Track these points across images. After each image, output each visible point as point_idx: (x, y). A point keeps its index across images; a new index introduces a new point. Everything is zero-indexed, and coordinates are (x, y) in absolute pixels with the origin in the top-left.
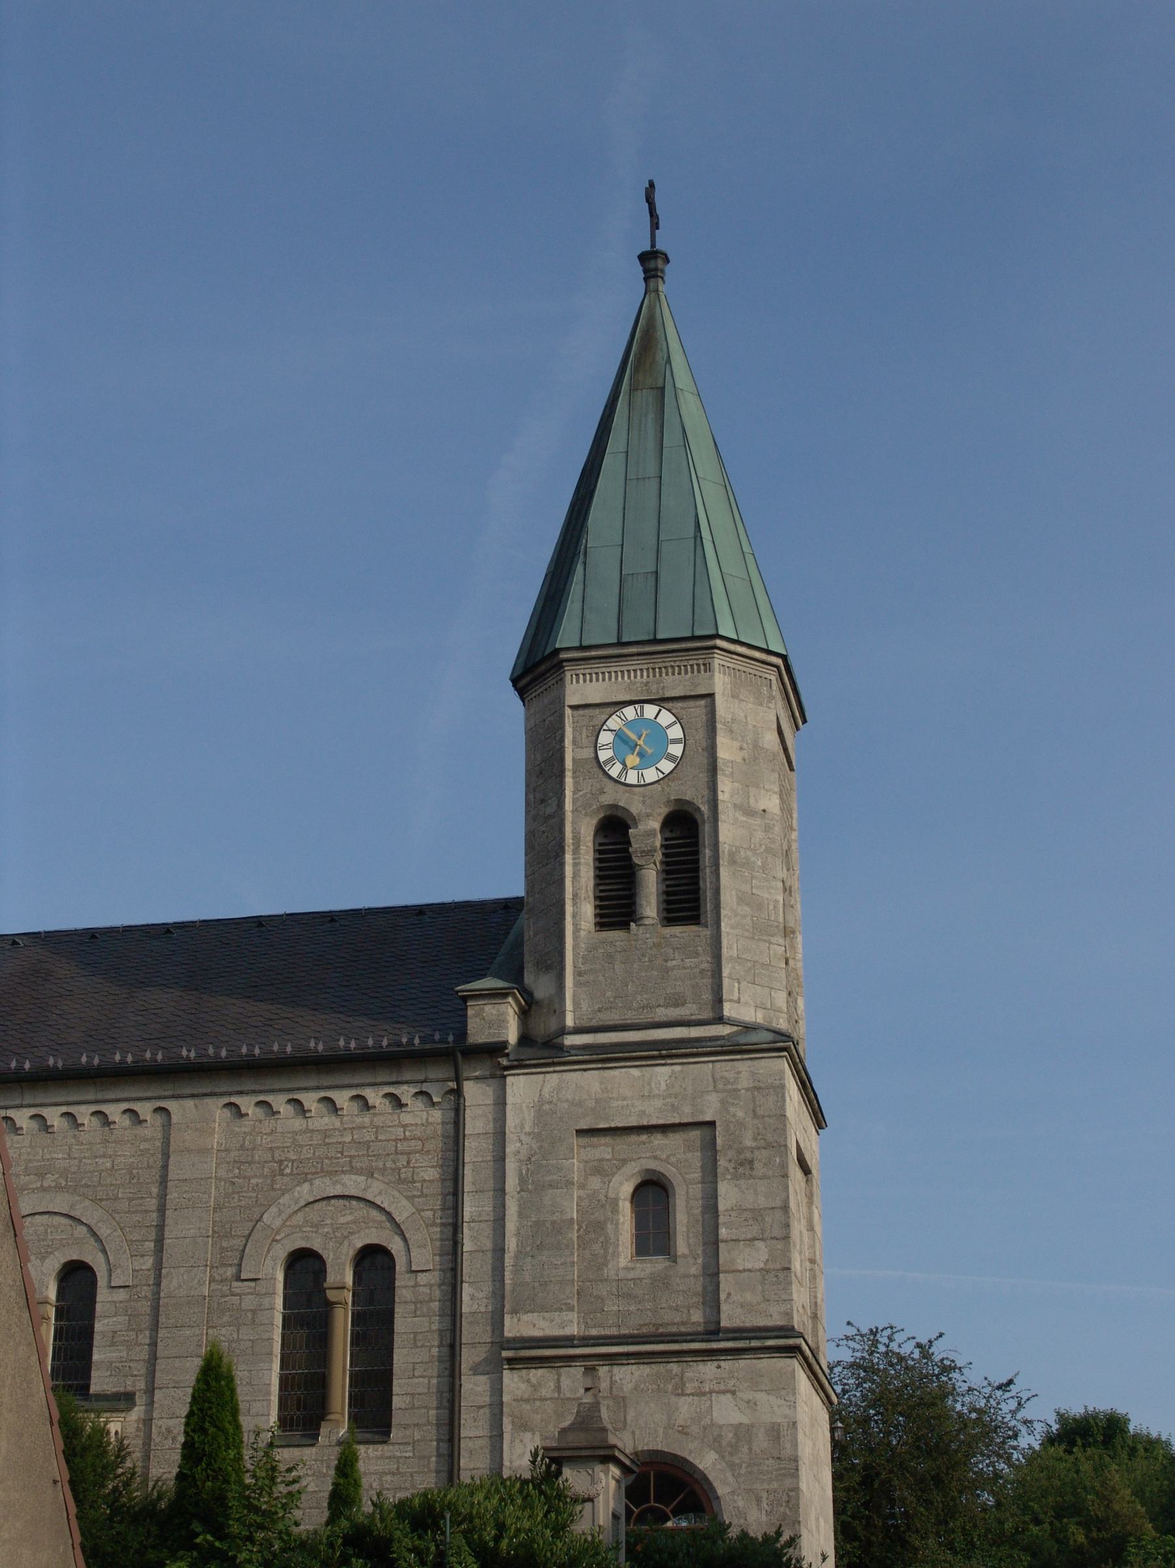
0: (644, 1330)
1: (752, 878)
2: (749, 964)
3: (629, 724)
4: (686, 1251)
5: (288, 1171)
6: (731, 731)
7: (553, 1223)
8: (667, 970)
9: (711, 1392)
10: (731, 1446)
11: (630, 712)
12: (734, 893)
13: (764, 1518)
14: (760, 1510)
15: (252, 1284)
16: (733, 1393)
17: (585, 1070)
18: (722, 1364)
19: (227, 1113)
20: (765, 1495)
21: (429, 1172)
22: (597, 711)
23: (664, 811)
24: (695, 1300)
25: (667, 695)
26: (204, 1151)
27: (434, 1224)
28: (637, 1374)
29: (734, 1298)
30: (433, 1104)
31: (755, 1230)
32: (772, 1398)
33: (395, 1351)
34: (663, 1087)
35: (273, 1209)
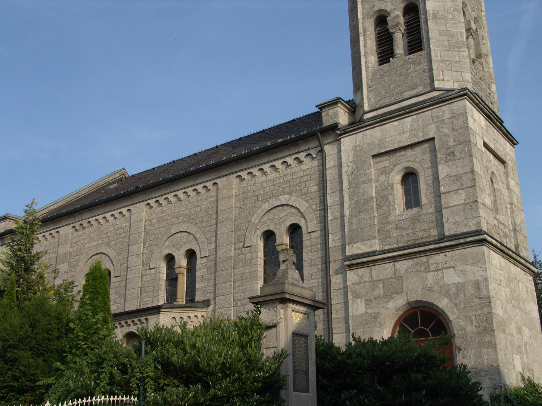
0: (409, 243)
2: (448, 62)
4: (426, 202)
5: (260, 199)
7: (364, 200)
9: (442, 269)
12: (437, 31)
13: (475, 330)
14: (472, 326)
15: (249, 248)
16: (454, 267)
17: (373, 128)
18: (447, 254)
19: (238, 179)
20: (474, 318)
21: (314, 188)
24: (432, 225)
26: (230, 197)
27: (317, 210)
28: (406, 264)
30: (314, 158)
31: (457, 185)
32: (474, 268)
34: (409, 127)
35: (255, 216)
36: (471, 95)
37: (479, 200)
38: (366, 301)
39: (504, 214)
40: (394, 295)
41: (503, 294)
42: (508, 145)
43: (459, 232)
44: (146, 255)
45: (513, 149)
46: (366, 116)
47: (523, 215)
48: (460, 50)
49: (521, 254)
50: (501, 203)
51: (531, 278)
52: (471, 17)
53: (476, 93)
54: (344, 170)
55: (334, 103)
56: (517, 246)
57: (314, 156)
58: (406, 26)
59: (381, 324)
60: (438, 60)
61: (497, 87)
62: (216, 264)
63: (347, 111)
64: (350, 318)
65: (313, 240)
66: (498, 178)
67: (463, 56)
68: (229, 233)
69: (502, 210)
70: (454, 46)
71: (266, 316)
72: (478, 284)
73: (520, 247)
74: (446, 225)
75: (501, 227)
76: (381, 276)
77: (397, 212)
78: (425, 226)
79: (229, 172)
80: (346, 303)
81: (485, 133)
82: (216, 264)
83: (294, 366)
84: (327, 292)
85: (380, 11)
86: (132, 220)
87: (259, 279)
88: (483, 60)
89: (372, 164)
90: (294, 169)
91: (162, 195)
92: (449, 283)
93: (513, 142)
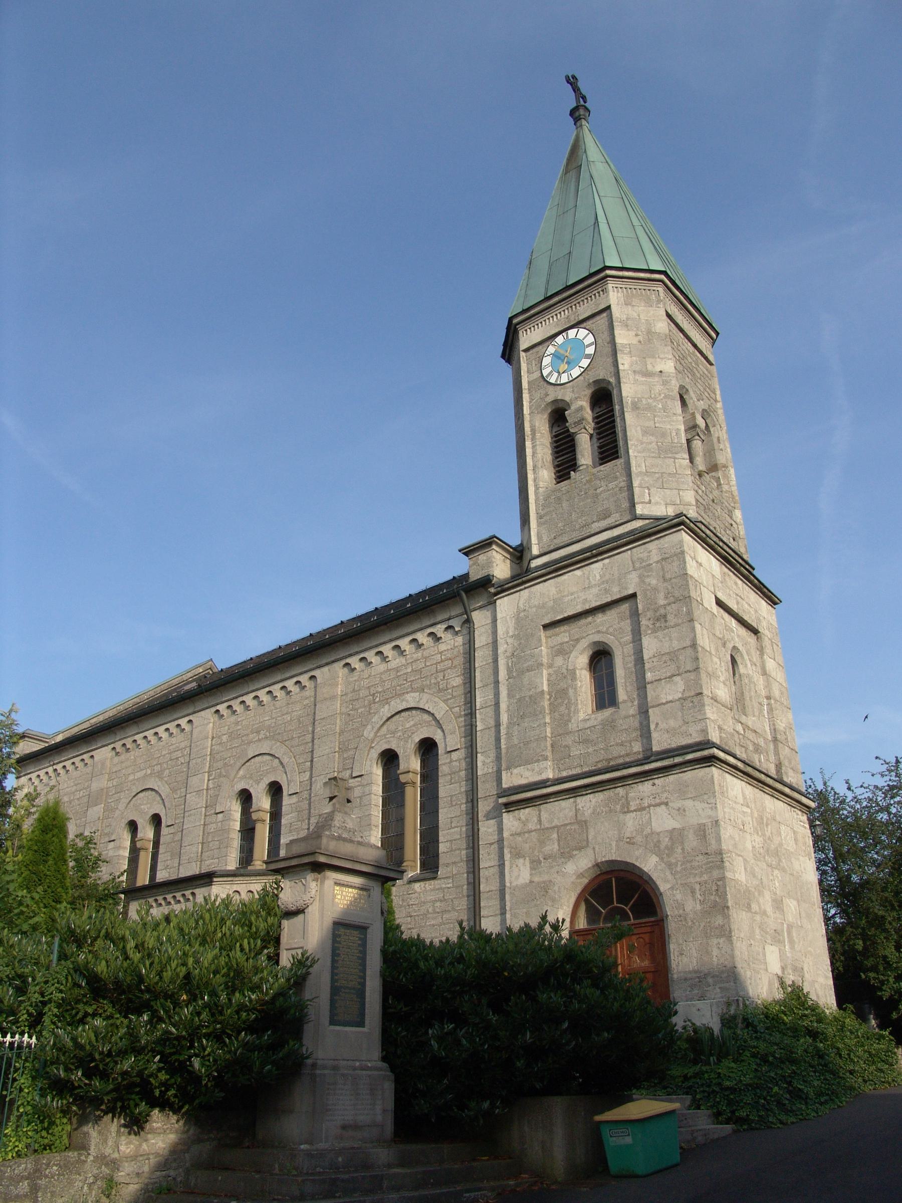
0: (600, 766)
1: (655, 416)
2: (657, 475)
3: (560, 346)
4: (625, 698)
5: (377, 699)
6: (627, 326)
7: (530, 697)
8: (597, 496)
9: (649, 807)
10: (668, 850)
11: (560, 340)
12: (639, 428)
13: (698, 907)
14: (695, 900)
15: (359, 779)
16: (667, 804)
17: (545, 581)
18: (656, 781)
19: (346, 670)
20: (697, 887)
21: (456, 680)
22: (540, 347)
23: (588, 392)
24: (634, 735)
25: (581, 318)
26: (333, 698)
27: (460, 716)
28: (594, 801)
29: (661, 726)
30: (457, 633)
31: (672, 669)
32: (697, 803)
33: (440, 811)
34: (598, 577)
35: (369, 727)
36: (692, 525)
37: (705, 692)
38: (532, 862)
39: (757, 714)
40: (575, 852)
41: (749, 846)
42: (763, 604)
43: (674, 745)
44: (211, 792)
45: (774, 611)
46: (534, 564)
47: (790, 715)
48: (677, 456)
49: (785, 779)
50: (751, 697)
51: (805, 818)
52: (696, 409)
53: (701, 522)
54: (501, 650)
55: (486, 544)
56: (779, 766)
57: (457, 629)
58: (597, 423)
59: (553, 900)
60: (641, 472)
61: (743, 515)
62: (310, 804)
63: (508, 556)
64: (507, 891)
65: (454, 763)
66: (746, 657)
67: (681, 466)
68: (330, 755)
69: (753, 707)
70: (665, 451)
71: (290, 893)
72: (704, 831)
73: (783, 768)
74: (655, 735)
75: (750, 735)
76: (556, 820)
77: (582, 716)
78: (624, 737)
79: (333, 659)
80: (502, 866)
81: (720, 585)
82: (310, 804)
83: (333, 980)
84: (473, 848)
85: (556, 401)
86: (194, 736)
87: (374, 828)
88: (720, 474)
89: (544, 640)
90: (428, 651)
91: (236, 698)
92: (659, 830)
93: (772, 600)
